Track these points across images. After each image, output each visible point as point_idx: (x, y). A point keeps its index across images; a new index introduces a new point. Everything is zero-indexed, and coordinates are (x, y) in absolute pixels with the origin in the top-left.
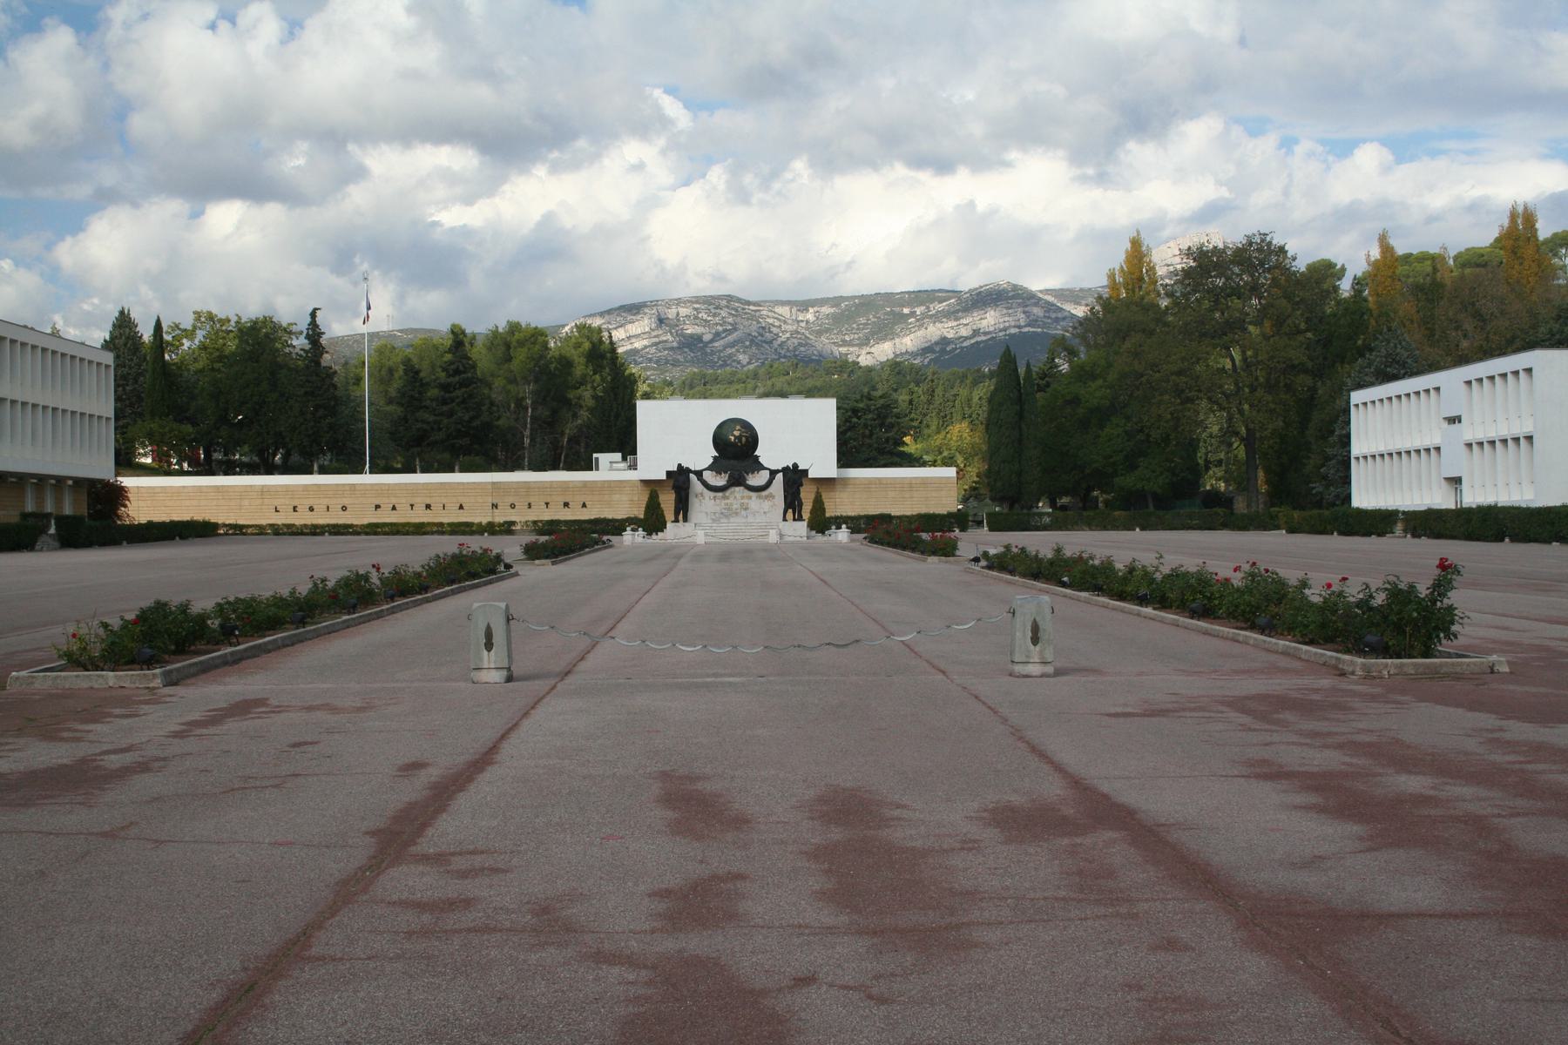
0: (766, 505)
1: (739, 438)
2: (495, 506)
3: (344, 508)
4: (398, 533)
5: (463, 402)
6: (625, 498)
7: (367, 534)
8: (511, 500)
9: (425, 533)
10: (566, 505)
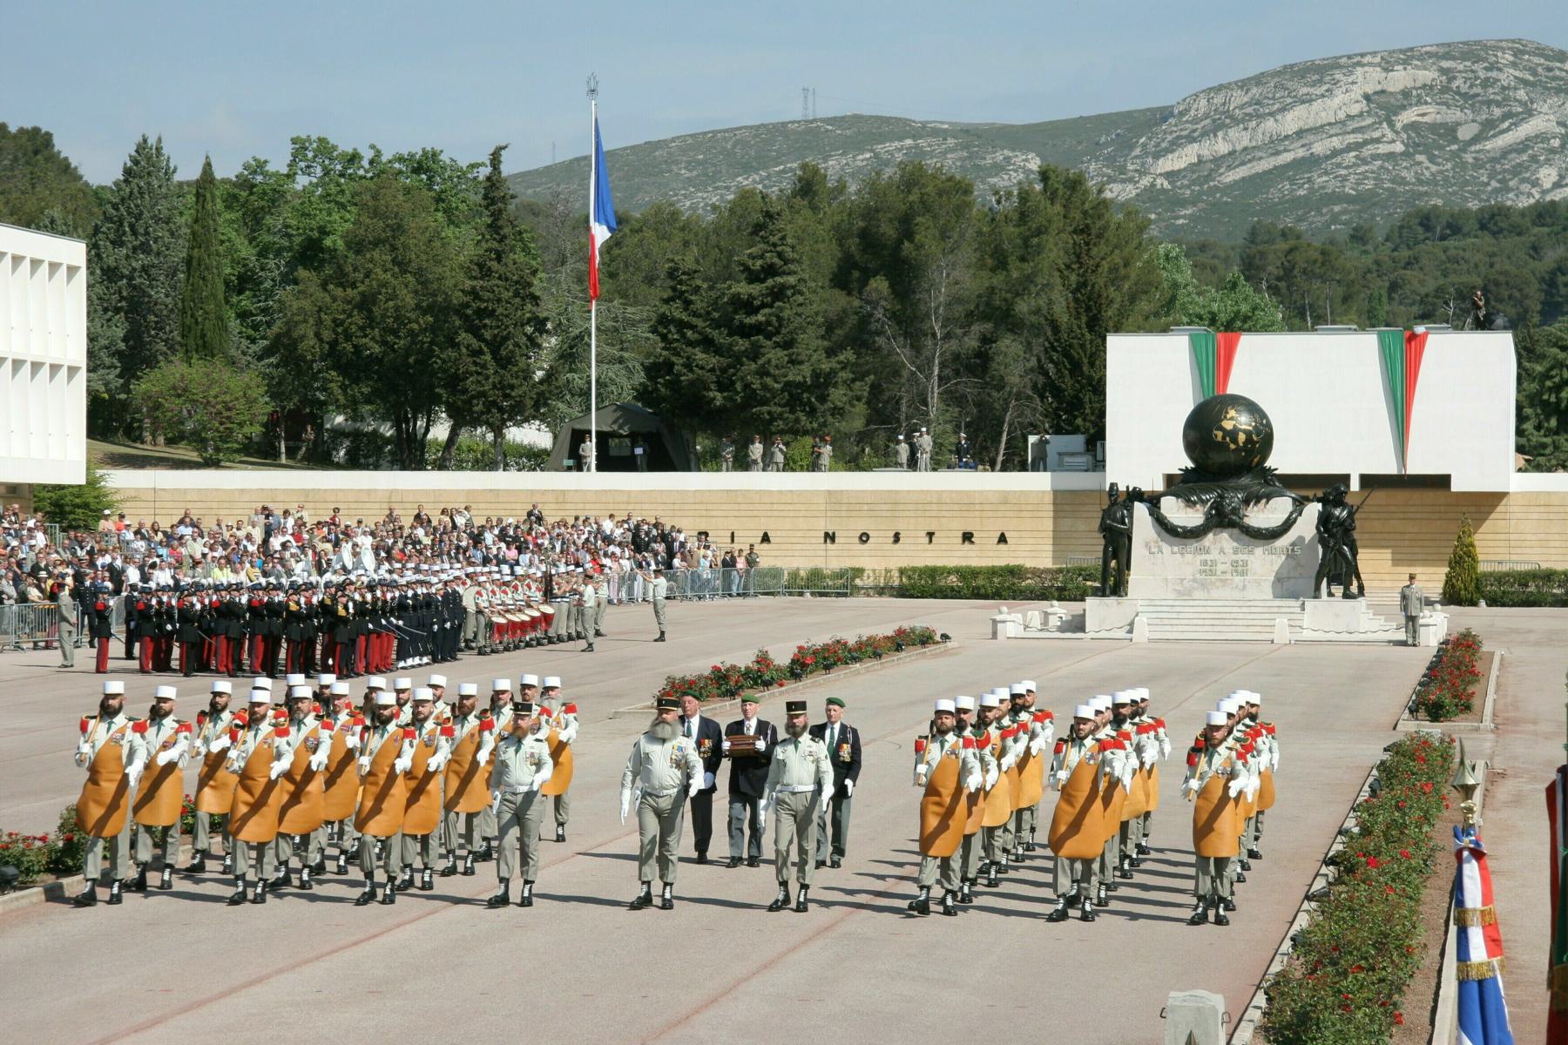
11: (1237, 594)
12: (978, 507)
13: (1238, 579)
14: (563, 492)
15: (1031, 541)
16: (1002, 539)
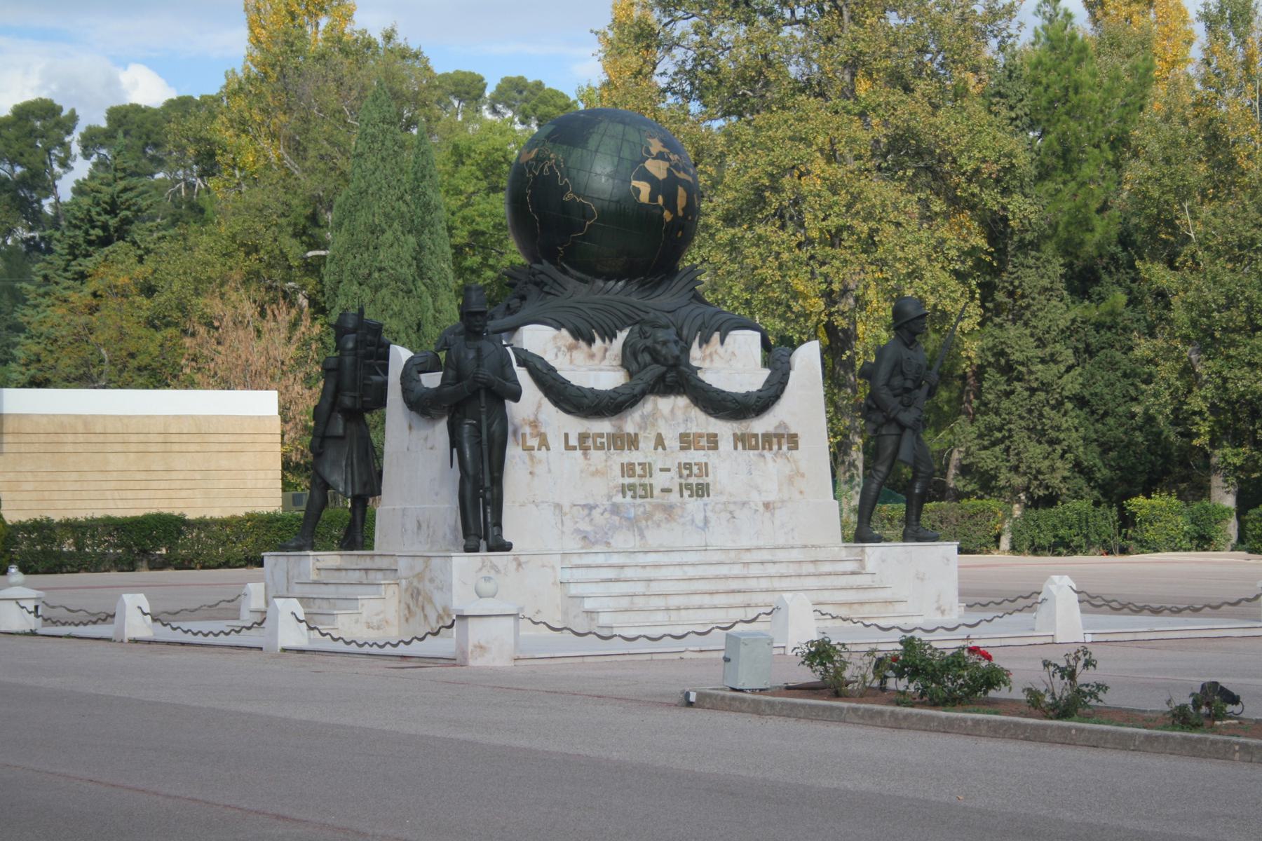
11: (696, 540)
13: (694, 505)
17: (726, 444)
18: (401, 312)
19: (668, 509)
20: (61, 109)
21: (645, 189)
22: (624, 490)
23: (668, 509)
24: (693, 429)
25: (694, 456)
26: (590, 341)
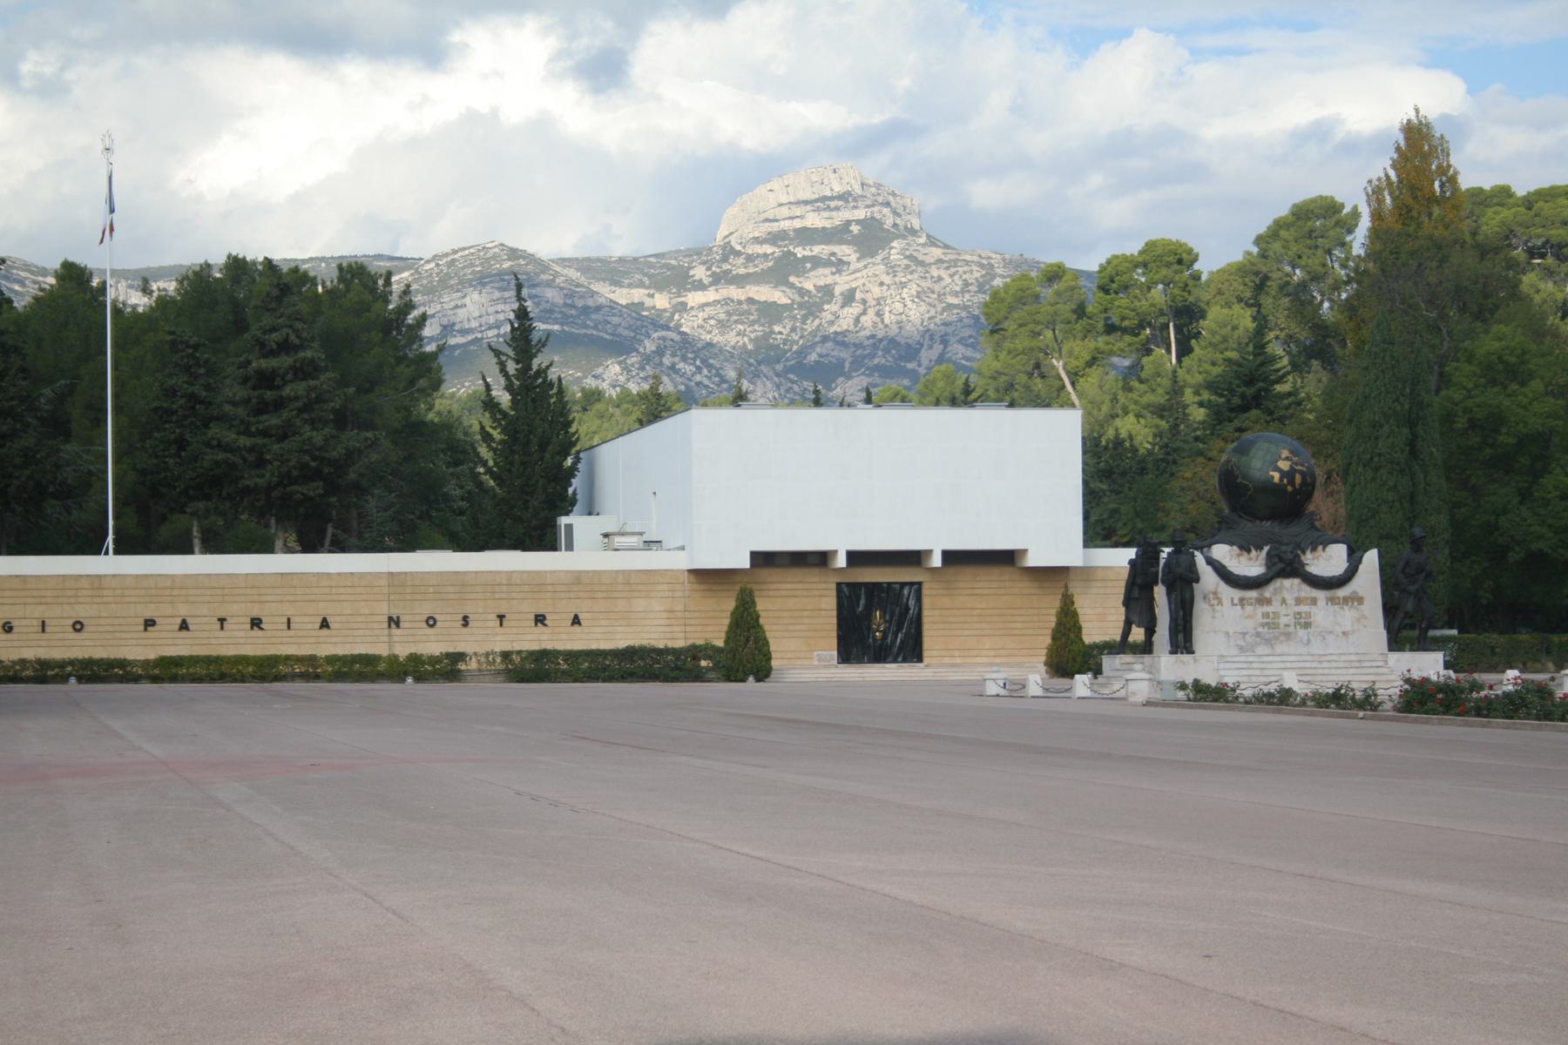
0: (1347, 616)
1: (1289, 475)
2: (394, 622)
3: (78, 626)
4: (222, 678)
5: (306, 408)
6: (657, 606)
7: (155, 679)
8: (427, 609)
9: (278, 678)
10: (540, 619)
11: (1303, 650)
12: (550, 588)
13: (1302, 633)
14: (100, 577)
15: (604, 623)
16: (576, 621)
17: (1321, 603)
18: (1395, 487)
19: (1288, 635)
20: (1342, 206)
21: (1276, 476)
22: (1263, 625)
23: (1288, 635)
24: (1303, 594)
25: (1304, 608)
26: (1249, 551)
